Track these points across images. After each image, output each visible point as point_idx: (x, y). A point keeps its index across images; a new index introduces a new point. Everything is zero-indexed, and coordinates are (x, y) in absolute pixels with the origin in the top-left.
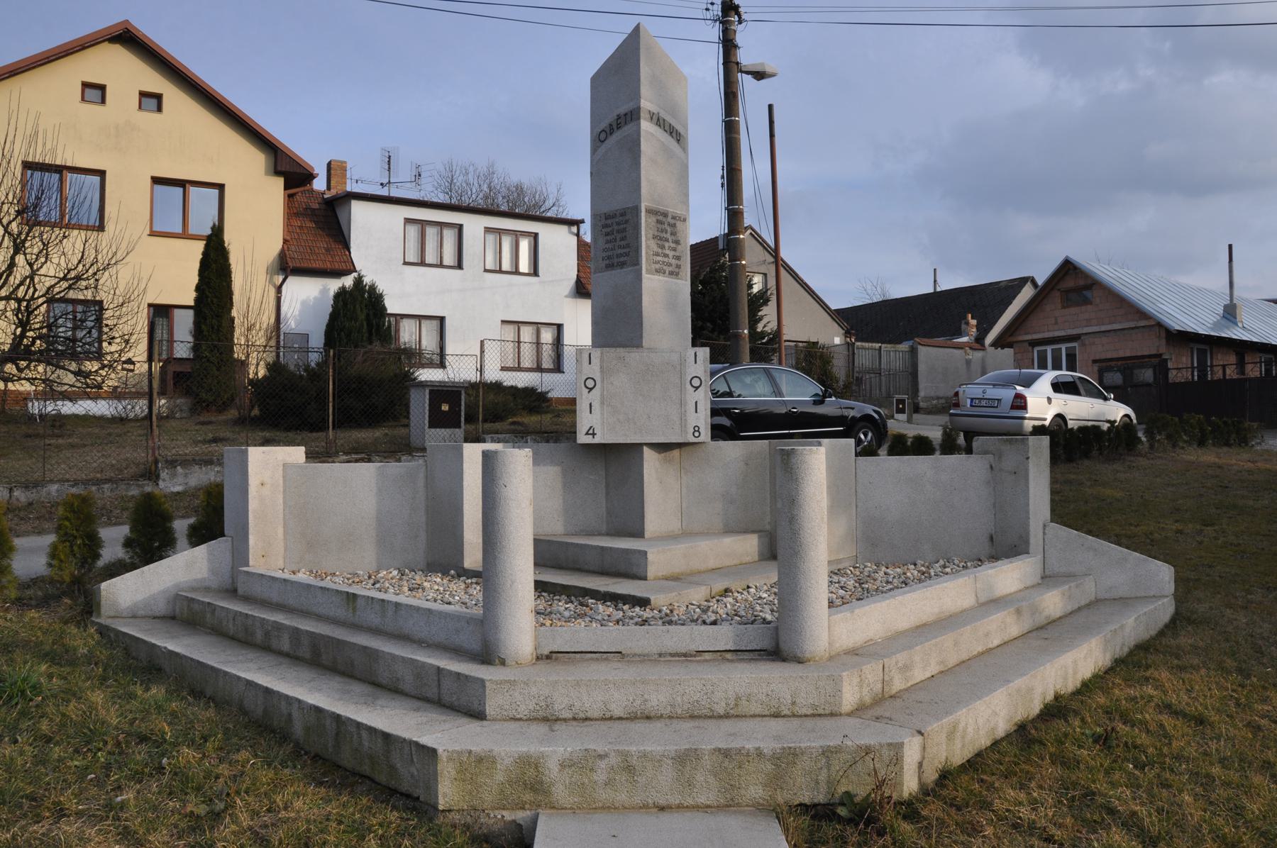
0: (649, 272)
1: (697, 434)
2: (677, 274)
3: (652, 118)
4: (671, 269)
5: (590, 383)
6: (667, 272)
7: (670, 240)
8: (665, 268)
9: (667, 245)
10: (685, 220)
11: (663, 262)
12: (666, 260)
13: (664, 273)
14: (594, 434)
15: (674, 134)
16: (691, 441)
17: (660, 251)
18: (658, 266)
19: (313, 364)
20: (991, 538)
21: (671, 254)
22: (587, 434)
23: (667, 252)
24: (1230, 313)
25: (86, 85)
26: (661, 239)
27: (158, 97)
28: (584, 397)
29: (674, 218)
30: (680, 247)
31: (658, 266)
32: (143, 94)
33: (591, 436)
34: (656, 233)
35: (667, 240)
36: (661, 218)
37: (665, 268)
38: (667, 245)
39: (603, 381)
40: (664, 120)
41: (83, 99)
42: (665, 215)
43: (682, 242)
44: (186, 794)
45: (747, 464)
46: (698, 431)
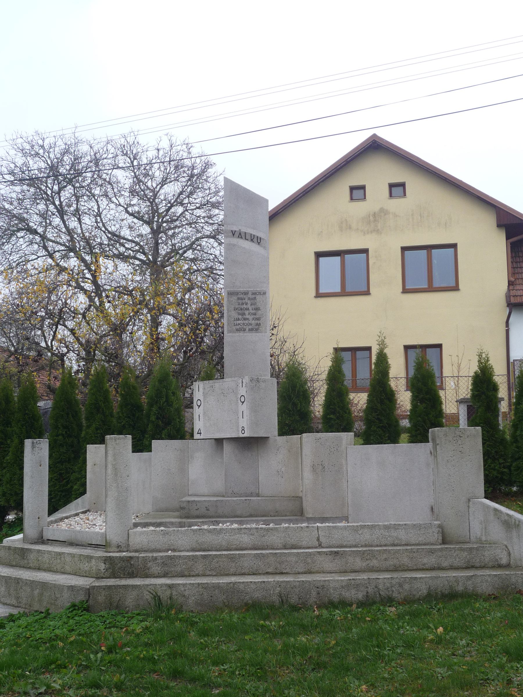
0: (229, 331)
1: (243, 432)
2: (257, 330)
3: (233, 235)
4: (250, 327)
5: (199, 404)
6: (247, 329)
7: (250, 309)
8: (244, 327)
9: (247, 312)
10: (264, 293)
11: (244, 324)
12: (247, 322)
13: (245, 330)
14: (200, 433)
15: (255, 240)
16: (241, 436)
17: (240, 317)
18: (238, 327)
19: (283, 365)
20: (432, 508)
21: (250, 317)
22: (198, 433)
23: (247, 317)
24: (359, 359)
25: (352, 189)
26: (241, 309)
27: (402, 185)
28: (197, 411)
29: (254, 294)
30: (259, 312)
31: (238, 327)
32: (392, 186)
33: (199, 434)
34: (237, 307)
35: (248, 309)
36: (242, 296)
37: (244, 327)
38: (247, 312)
39: (204, 402)
40: (260, 238)
41: (352, 199)
42: (246, 293)
43: (261, 308)
44: (482, 621)
45: (289, 451)
46: (244, 430)
